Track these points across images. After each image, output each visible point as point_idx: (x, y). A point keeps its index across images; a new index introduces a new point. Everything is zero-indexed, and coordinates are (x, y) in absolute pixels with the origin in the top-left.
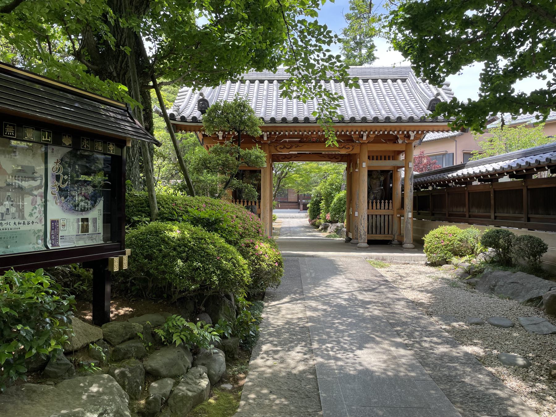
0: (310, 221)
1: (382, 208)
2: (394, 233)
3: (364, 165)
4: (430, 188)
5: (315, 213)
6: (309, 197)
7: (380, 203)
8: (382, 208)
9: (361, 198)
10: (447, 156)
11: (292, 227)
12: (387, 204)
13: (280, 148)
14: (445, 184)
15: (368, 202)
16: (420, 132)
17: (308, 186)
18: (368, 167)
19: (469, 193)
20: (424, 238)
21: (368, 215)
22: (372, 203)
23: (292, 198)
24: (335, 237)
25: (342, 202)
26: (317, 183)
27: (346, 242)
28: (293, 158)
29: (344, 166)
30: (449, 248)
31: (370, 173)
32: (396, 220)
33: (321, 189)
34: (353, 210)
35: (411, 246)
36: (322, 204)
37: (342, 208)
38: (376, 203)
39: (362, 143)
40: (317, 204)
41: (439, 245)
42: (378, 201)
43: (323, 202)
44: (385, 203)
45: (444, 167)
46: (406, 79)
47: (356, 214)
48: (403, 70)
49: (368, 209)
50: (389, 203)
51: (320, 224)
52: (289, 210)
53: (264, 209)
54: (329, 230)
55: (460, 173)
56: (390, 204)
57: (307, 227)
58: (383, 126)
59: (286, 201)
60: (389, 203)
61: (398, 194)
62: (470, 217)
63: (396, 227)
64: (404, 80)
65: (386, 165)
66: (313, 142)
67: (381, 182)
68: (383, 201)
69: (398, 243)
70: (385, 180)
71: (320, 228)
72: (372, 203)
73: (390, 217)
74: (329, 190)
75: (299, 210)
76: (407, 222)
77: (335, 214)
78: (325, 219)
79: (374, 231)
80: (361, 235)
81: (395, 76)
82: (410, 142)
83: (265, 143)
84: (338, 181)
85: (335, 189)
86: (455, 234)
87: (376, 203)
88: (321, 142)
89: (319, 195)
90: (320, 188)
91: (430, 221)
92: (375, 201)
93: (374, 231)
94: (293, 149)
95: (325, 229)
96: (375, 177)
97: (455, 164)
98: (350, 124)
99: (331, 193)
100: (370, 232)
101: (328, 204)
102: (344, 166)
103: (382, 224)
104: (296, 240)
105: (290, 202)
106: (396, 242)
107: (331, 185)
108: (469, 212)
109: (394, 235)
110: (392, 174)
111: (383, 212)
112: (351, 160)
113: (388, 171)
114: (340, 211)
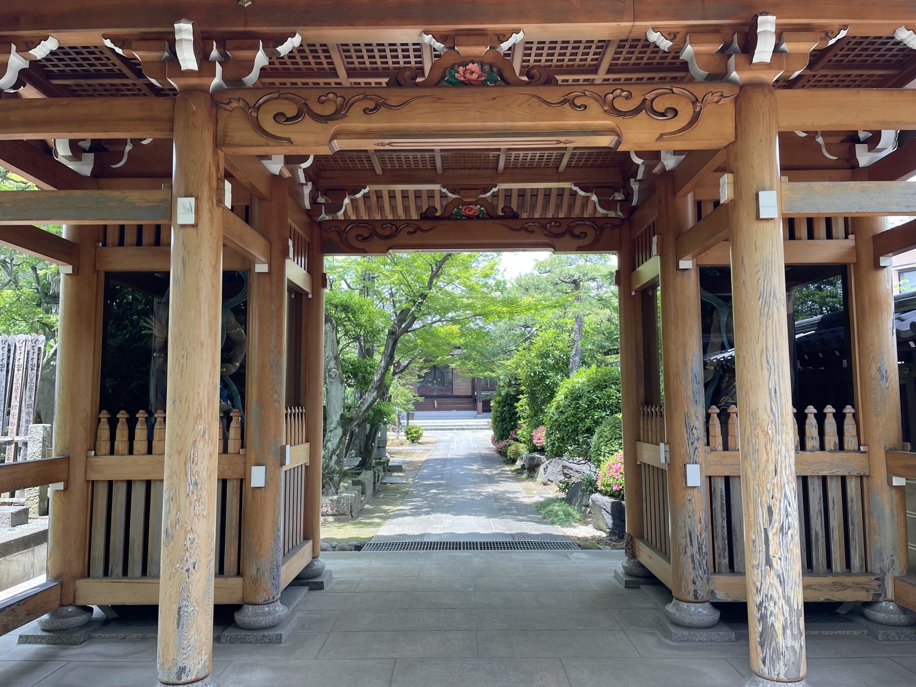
0: (495, 441)
2: (875, 566)
5: (506, 426)
6: (491, 385)
11: (451, 461)
12: (830, 424)
17: (488, 359)
23: (461, 387)
25: (583, 403)
26: (508, 353)
28: (403, 238)
36: (523, 405)
37: (582, 420)
39: (745, 88)
40: (510, 401)
43: (524, 400)
44: (821, 418)
50: (840, 418)
51: (517, 454)
52: (454, 412)
56: (849, 426)
57: (485, 460)
59: (449, 394)
60: (840, 418)
61: (884, 377)
71: (519, 464)
73: (853, 487)
74: (538, 369)
75: (475, 413)
83: (189, 91)
84: (560, 345)
85: (553, 368)
89: (514, 381)
94: (356, 122)
95: (531, 469)
99: (545, 378)
101: (537, 409)
104: (431, 566)
105: (458, 397)
106: (887, 610)
107: (544, 355)
109: (881, 579)
114: (576, 431)
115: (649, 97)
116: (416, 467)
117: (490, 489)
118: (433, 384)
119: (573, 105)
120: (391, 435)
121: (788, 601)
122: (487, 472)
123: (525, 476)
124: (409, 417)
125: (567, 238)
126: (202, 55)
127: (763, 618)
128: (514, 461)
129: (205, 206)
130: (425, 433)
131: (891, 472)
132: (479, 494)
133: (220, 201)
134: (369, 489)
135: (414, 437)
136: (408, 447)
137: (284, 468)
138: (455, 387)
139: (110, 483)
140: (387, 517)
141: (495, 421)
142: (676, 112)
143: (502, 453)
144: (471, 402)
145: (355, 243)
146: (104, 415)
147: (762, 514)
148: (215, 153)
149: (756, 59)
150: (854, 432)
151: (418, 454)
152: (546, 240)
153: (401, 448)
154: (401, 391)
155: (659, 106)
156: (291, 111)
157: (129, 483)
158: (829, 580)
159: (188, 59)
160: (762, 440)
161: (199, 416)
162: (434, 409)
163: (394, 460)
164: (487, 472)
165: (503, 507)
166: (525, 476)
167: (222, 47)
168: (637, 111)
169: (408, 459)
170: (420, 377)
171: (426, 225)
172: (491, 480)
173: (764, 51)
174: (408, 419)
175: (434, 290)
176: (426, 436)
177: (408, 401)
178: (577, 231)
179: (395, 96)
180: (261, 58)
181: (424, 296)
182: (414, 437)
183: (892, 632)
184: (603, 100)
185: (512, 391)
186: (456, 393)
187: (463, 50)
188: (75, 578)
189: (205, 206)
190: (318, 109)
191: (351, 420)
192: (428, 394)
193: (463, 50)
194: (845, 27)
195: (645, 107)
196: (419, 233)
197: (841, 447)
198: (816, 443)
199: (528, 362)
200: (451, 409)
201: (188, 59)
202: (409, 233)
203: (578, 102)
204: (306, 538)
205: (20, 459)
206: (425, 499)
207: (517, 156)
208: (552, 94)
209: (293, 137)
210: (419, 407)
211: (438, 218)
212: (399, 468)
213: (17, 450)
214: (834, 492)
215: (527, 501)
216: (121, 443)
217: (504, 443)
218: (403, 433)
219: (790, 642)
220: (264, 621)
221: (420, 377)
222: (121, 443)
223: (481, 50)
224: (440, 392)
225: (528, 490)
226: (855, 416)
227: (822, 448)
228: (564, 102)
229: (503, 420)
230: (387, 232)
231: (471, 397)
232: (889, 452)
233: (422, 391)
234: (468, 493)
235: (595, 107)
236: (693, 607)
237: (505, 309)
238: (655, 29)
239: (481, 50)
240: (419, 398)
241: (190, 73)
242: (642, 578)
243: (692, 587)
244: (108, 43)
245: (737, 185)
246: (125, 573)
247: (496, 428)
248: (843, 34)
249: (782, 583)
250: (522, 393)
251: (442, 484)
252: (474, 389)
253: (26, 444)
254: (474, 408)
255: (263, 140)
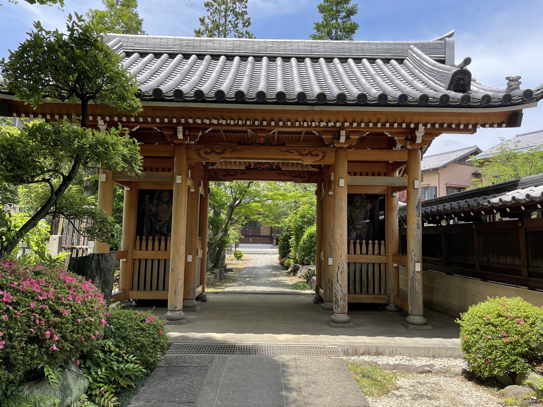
1: (370, 252)
3: (342, 183)
4: (444, 223)
5: (284, 252)
6: (279, 230)
7: (367, 244)
8: (370, 252)
9: (338, 237)
10: (429, 190)
11: (257, 268)
12: (376, 246)
13: (205, 153)
14: (475, 216)
15: (349, 243)
16: (437, 126)
17: (278, 217)
18: (349, 186)
19: (526, 233)
20: (459, 321)
21: (349, 264)
22: (355, 244)
23: (265, 231)
24: (304, 288)
26: (286, 215)
27: (315, 303)
29: (312, 187)
30: (519, 350)
31: (351, 198)
32: (391, 272)
33: (290, 221)
34: (325, 254)
35: (418, 319)
37: (313, 247)
38: (361, 244)
39: (338, 149)
41: (498, 343)
42: (364, 241)
44: (373, 244)
45: (427, 199)
46: (403, 60)
47: (330, 261)
48: (398, 47)
49: (348, 253)
50: (380, 244)
52: (261, 245)
53: (174, 253)
54: (299, 274)
55: (507, 197)
57: (274, 268)
58: (375, 113)
59: (258, 235)
60: (380, 244)
61: (393, 231)
62: (530, 275)
63: (391, 283)
64: (401, 61)
65: (375, 184)
66: (261, 145)
67: (367, 212)
68: (371, 241)
69: (395, 309)
70: (372, 211)
71: (290, 270)
72: (355, 244)
73: (383, 267)
74: (300, 223)
75: (271, 245)
76: (413, 279)
77: (304, 256)
78: (294, 259)
79: (358, 289)
80: (337, 299)
81: (388, 56)
82: (415, 147)
83: (180, 144)
84: (311, 212)
86: (527, 317)
87: (361, 244)
88: (272, 145)
90: (289, 221)
91: (444, 274)
92: (358, 241)
93: (358, 289)
95: (295, 271)
96: (358, 205)
97: (438, 197)
98: (317, 108)
99: (303, 227)
100: (352, 290)
101: (298, 239)
102: (312, 187)
103: (370, 278)
104: (245, 298)
106: (391, 307)
107: (303, 217)
108: (529, 266)
110: (384, 199)
111: (371, 258)
112: (321, 177)
113: (376, 196)
114: (310, 251)
115: (311, 150)
116: (239, 270)
117: (274, 279)
118: (250, 229)
119: (290, 152)
120: (227, 256)
121: (342, 291)
122: (274, 273)
123: (292, 274)
124: (236, 246)
125: (298, 178)
126: (184, 135)
127: (336, 296)
128: (288, 268)
129: (184, 177)
130: (244, 255)
131: (393, 263)
132: (269, 281)
133: (188, 176)
134: (218, 277)
135: (238, 257)
136: (235, 261)
137: (198, 257)
138: (261, 231)
139: (140, 260)
140: (227, 286)
141: (280, 249)
142: (318, 155)
143: (282, 264)
144: (269, 239)
145: (221, 177)
146: (138, 237)
147: (337, 268)
148: (187, 162)
149: (341, 141)
150: (384, 249)
151: (240, 265)
152: (291, 179)
153: (232, 262)
154: (233, 233)
155: (314, 153)
156: (209, 151)
157: (146, 260)
158: (373, 296)
159: (180, 136)
160: (338, 248)
161: (181, 237)
162: (249, 243)
163: (228, 267)
164: (274, 273)
165: (277, 284)
166: (292, 274)
167: (189, 131)
168: (307, 154)
169: (236, 267)
170: (242, 225)
171: (247, 172)
172: (275, 276)
173: (343, 139)
174: (236, 247)
175: (250, 189)
176: (245, 257)
177: (236, 238)
178: (302, 176)
179: (239, 148)
180: (200, 134)
181: (246, 192)
182: (238, 257)
183: (391, 313)
184: (298, 151)
185: (288, 234)
186: (262, 234)
187: (259, 135)
188: (128, 290)
189: (184, 177)
190: (217, 151)
191: (212, 244)
192: (246, 234)
193: (259, 135)
194: (368, 131)
195: (310, 153)
196: (245, 175)
197: (380, 254)
198: (372, 253)
199: (296, 220)
200: (259, 243)
201: (180, 136)
202: (241, 174)
203: (291, 151)
204: (201, 284)
205: (84, 255)
206: (244, 282)
207: (289, 136)
208: (284, 149)
209: (209, 158)
210: (242, 241)
211: (252, 169)
212: (231, 270)
213: (83, 252)
214: (377, 268)
215: (291, 284)
216: (144, 247)
217: (283, 260)
218: (233, 255)
219: (342, 303)
220: (191, 305)
221: (242, 225)
222: (144, 247)
223: (264, 135)
224: (253, 234)
225: (292, 280)
226: (385, 244)
227: (373, 254)
228: (287, 151)
229: (284, 248)
230: (233, 174)
231: (270, 237)
232: (394, 255)
233: (243, 232)
234: (263, 280)
235: (296, 153)
236: (340, 316)
237: (281, 197)
238: (314, 130)
239: (264, 135)
240: (242, 237)
241: (181, 139)
242: (319, 300)
243: (329, 297)
244: (155, 128)
245: (335, 176)
246: (144, 289)
247: (280, 253)
248: (368, 133)
249: (341, 287)
250: (292, 234)
251: (252, 275)
252: (272, 232)
253: (87, 249)
254: (272, 243)
255: (200, 158)
